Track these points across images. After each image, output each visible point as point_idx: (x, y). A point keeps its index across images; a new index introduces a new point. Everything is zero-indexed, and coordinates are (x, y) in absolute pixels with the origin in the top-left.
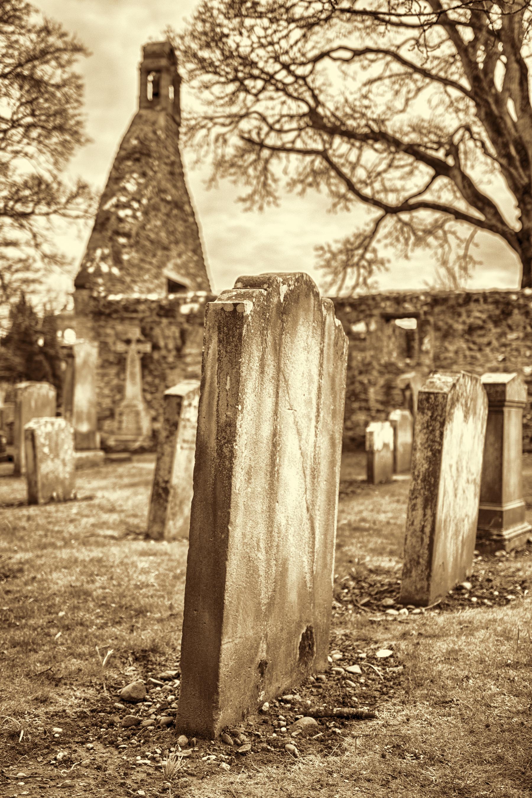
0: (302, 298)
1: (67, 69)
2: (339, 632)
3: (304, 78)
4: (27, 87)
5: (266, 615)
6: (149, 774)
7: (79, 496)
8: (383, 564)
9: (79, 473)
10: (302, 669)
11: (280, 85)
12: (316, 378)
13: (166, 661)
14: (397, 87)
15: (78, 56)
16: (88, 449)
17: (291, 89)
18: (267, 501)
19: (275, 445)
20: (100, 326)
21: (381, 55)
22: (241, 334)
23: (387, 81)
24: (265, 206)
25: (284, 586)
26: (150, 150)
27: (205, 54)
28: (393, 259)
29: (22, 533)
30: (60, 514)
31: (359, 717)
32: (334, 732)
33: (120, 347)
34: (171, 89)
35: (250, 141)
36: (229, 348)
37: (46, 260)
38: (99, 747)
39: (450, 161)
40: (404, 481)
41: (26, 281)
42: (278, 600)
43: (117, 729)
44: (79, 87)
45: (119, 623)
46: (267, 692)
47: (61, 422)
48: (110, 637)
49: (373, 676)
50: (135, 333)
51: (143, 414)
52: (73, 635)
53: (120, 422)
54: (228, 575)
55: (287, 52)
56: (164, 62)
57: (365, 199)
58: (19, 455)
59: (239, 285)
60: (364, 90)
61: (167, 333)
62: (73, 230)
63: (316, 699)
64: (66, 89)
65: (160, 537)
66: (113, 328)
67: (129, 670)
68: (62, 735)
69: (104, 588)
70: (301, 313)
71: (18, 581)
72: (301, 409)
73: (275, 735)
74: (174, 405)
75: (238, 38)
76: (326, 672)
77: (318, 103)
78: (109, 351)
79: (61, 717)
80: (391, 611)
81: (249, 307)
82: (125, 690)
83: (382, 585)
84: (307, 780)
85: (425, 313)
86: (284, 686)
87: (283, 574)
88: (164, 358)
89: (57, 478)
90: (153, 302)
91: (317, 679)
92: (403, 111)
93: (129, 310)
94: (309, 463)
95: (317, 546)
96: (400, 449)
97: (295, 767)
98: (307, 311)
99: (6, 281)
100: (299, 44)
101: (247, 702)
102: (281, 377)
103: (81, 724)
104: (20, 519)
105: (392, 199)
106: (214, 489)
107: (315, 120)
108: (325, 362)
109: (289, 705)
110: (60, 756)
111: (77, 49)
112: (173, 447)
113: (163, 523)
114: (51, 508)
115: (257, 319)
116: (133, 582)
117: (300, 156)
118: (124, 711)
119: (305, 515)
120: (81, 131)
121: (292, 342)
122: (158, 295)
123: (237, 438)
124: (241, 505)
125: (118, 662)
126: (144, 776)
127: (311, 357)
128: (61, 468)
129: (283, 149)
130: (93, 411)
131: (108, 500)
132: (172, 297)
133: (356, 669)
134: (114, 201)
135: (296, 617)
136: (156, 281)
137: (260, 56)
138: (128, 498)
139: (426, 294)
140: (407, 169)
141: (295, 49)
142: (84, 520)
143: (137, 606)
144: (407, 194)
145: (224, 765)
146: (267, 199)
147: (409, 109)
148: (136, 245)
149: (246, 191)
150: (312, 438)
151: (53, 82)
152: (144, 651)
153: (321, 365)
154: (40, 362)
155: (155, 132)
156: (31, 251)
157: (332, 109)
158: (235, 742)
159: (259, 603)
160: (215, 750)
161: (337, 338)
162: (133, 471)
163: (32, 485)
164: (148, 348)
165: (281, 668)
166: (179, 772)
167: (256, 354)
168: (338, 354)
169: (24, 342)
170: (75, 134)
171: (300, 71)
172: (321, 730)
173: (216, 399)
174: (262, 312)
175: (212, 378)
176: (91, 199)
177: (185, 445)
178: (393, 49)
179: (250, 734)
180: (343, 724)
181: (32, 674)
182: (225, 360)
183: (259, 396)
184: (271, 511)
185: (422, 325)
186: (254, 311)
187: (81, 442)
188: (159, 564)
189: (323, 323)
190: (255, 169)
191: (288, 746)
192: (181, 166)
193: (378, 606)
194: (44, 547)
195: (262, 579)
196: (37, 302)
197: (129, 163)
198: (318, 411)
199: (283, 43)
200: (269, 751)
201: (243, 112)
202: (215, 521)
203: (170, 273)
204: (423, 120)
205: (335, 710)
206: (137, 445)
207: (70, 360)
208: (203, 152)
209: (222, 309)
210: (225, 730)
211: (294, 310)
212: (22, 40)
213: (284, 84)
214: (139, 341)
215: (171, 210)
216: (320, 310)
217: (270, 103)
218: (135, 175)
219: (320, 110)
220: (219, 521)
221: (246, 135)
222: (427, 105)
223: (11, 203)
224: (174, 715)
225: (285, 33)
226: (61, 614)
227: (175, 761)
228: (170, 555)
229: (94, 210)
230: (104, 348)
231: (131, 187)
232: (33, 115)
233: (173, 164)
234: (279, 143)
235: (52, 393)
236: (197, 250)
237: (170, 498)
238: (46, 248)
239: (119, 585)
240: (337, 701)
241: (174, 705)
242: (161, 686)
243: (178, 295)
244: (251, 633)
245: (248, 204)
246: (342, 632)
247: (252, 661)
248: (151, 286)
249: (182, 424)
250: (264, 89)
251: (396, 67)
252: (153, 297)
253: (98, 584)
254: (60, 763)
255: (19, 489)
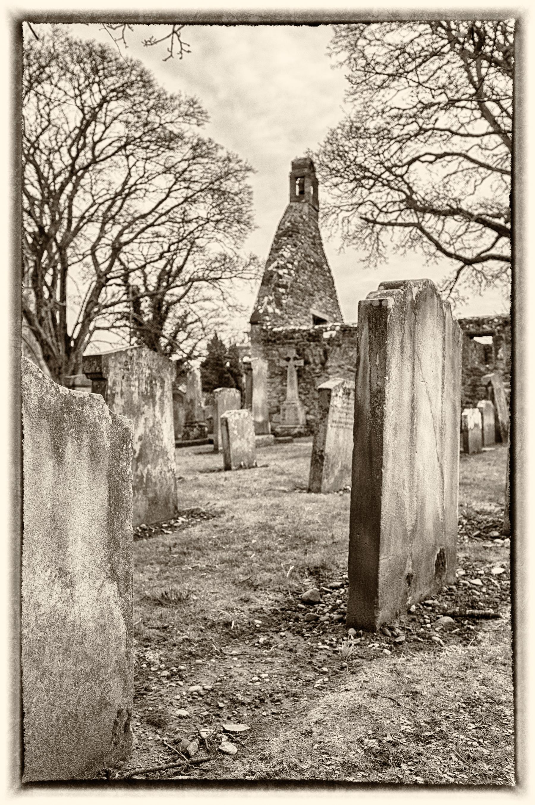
0: (428, 298)
1: (242, 182)
2: (461, 555)
3: (402, 176)
4: (216, 196)
5: (410, 539)
6: (329, 656)
7: (259, 465)
8: (485, 508)
9: (258, 449)
10: (438, 581)
11: (385, 182)
12: (441, 359)
13: (333, 575)
14: (467, 178)
15: (249, 174)
16: (263, 434)
17: (393, 184)
18: (409, 451)
19: (413, 408)
20: (269, 350)
21: (455, 157)
22: (386, 323)
23: (460, 174)
24: (378, 264)
25: (423, 517)
26: (299, 232)
27: (332, 165)
28: (471, 296)
29: (222, 489)
30: (246, 476)
31: (487, 617)
32: (469, 628)
33: (283, 363)
34: (312, 189)
35: (367, 220)
36: (377, 334)
37: (230, 308)
38: (289, 635)
39: (508, 226)
40: (491, 451)
41: (217, 324)
42: (419, 528)
43: (300, 623)
44: (250, 193)
45: (296, 548)
46: (413, 598)
47: (245, 412)
48: (291, 557)
49: (492, 587)
50: (293, 353)
51: (299, 409)
52: (264, 556)
53: (284, 415)
54: (383, 507)
55: (389, 160)
56: (306, 171)
57: (449, 255)
58: (217, 438)
59: (382, 288)
60: (446, 180)
61: (314, 353)
62: (248, 287)
63: (451, 604)
64: (241, 195)
65: (318, 491)
66: (278, 350)
67: (306, 581)
68: (262, 625)
69: (283, 524)
70: (428, 309)
71: (222, 519)
72: (431, 383)
73: (422, 630)
74: (326, 396)
75: (355, 153)
76: (455, 584)
77: (412, 192)
78: (275, 366)
79: (260, 612)
80: (497, 540)
81: (391, 303)
82: (305, 595)
83: (488, 522)
84: (455, 664)
85: (499, 331)
86: (425, 594)
87: (422, 508)
88: (313, 369)
89: (243, 452)
90: (304, 331)
91: (450, 589)
92: (473, 194)
93: (287, 338)
94: (438, 423)
95: (446, 488)
96: (486, 428)
97: (443, 653)
98: (432, 307)
99: (205, 324)
100: (398, 154)
101: (399, 605)
102: (416, 357)
103: (275, 618)
104: (220, 479)
105: (468, 255)
106: (370, 442)
107: (410, 203)
108: (447, 347)
109: (430, 608)
110: (261, 640)
111: (248, 170)
112: (326, 426)
113: (320, 481)
114: (240, 472)
115: (397, 311)
116: (302, 520)
117: (401, 228)
118: (305, 610)
119: (437, 464)
120: (251, 222)
121: (423, 331)
122: (309, 326)
123: (386, 401)
124: (390, 453)
125: (297, 575)
126: (325, 657)
127: (437, 343)
128: (246, 445)
129: (390, 224)
130: (267, 407)
131: (279, 466)
132: (317, 327)
133: (478, 582)
134: (275, 264)
135: (432, 541)
136: (305, 317)
137: (370, 164)
138: (293, 465)
139: (499, 317)
140: (478, 233)
141: (395, 157)
142: (264, 480)
143: (308, 536)
144: (479, 251)
145: (386, 651)
146: (379, 259)
147: (476, 192)
148: (291, 293)
149: (365, 254)
150: (440, 405)
151: (233, 191)
152: (316, 568)
153: (444, 349)
154: (228, 378)
155: (301, 217)
156: (221, 303)
157: (423, 195)
158: (393, 634)
159: (406, 529)
160: (377, 640)
161: (454, 329)
162: (295, 448)
163: (227, 457)
164: (301, 363)
165: (423, 579)
166: (352, 655)
167: (398, 339)
168: (455, 341)
169: (217, 364)
170: (247, 224)
171: (399, 171)
172: (458, 627)
173: (369, 372)
174: (401, 306)
175: (365, 357)
176: (259, 266)
177: (334, 425)
178: (464, 152)
179: (403, 629)
180: (474, 622)
181: (237, 582)
182: (374, 342)
183: (401, 371)
184: (412, 458)
185: (496, 341)
186: (395, 305)
187: (260, 429)
188: (320, 508)
189: (444, 318)
190: (370, 239)
191: (434, 638)
192: (320, 239)
193: (487, 537)
194: (238, 497)
195: (407, 511)
196: (225, 338)
197: (285, 238)
198: (443, 384)
199: (386, 154)
200: (419, 641)
201: (360, 201)
202: (371, 465)
203: (315, 311)
204: (487, 200)
205: (468, 611)
206: (296, 431)
207: (249, 372)
208: (334, 230)
209: (371, 304)
210: (384, 625)
211: (423, 306)
212: (213, 167)
213: (388, 181)
214: (295, 359)
215: (314, 268)
216: (442, 308)
217: (379, 195)
218: (289, 246)
219: (414, 196)
220: (374, 466)
221: (364, 216)
222: (489, 189)
223: (207, 272)
224: (344, 613)
225: (386, 147)
226: (254, 541)
227: (348, 646)
228: (327, 503)
229: (262, 270)
230: (272, 364)
231: (287, 254)
232: (220, 214)
233: (314, 237)
234: (386, 221)
235: (238, 395)
236: (333, 295)
237: (324, 463)
238: (230, 301)
239: (294, 522)
240: (467, 605)
241: (342, 606)
242: (331, 593)
243: (321, 326)
244: (400, 552)
245: (367, 263)
246: (463, 555)
247: (402, 573)
248: (302, 321)
249: (331, 409)
250: (374, 185)
251: (467, 164)
252: (304, 328)
253: (278, 521)
254: (262, 645)
255: (218, 461)
